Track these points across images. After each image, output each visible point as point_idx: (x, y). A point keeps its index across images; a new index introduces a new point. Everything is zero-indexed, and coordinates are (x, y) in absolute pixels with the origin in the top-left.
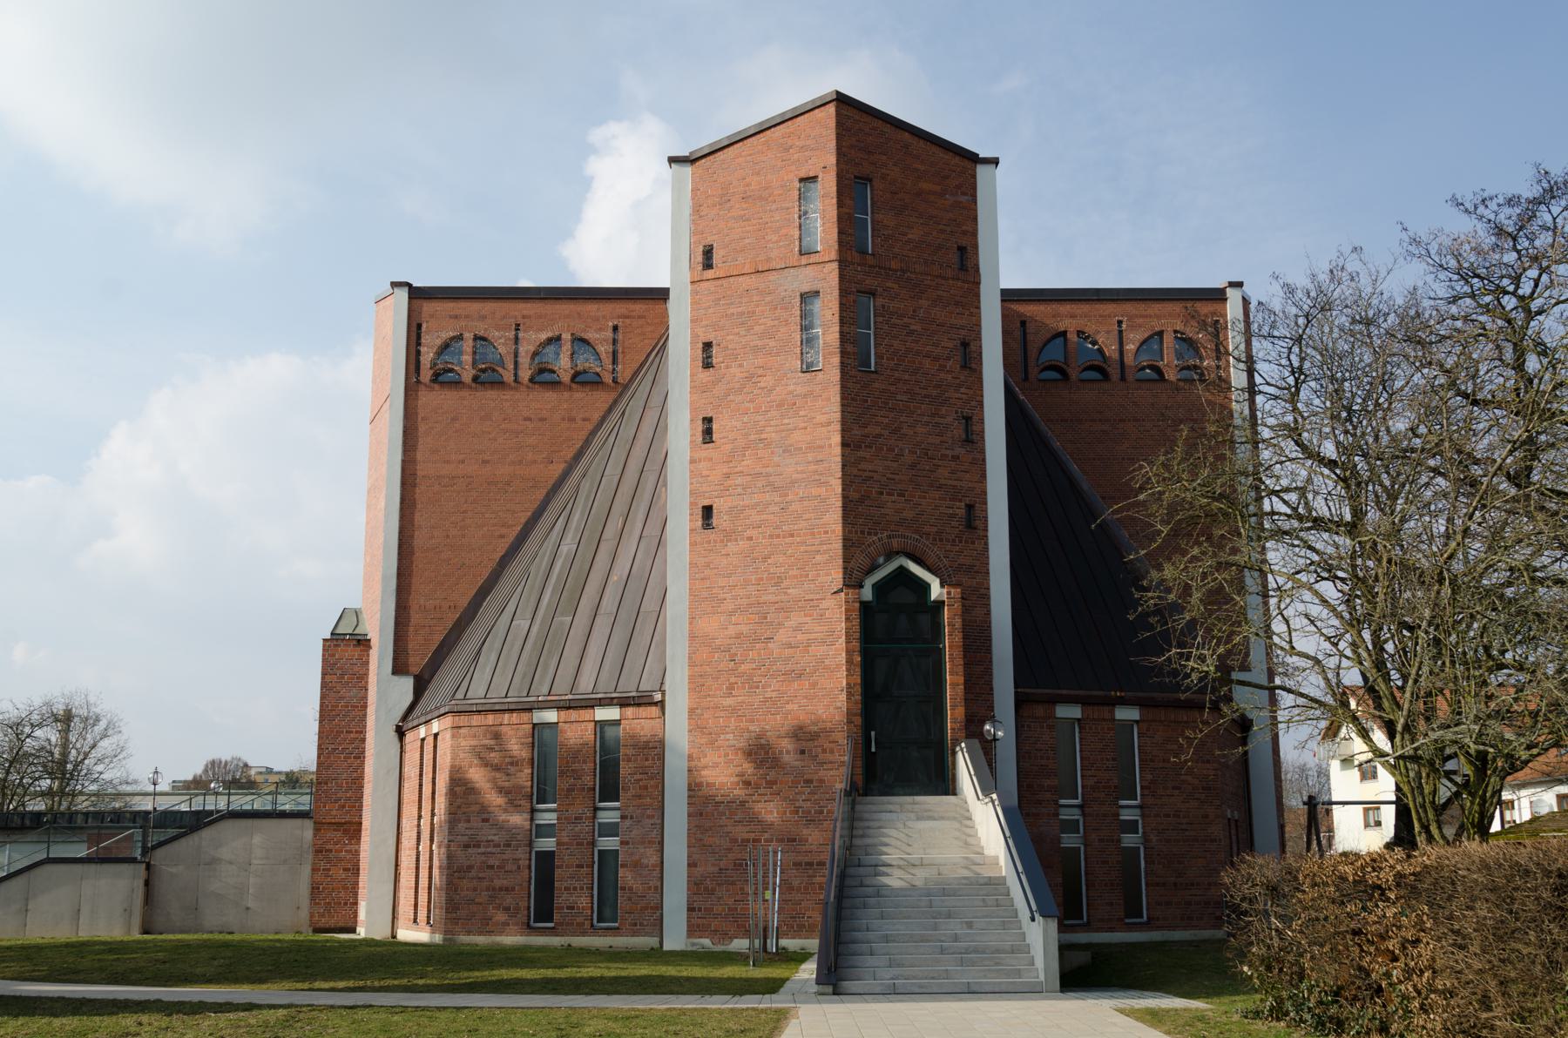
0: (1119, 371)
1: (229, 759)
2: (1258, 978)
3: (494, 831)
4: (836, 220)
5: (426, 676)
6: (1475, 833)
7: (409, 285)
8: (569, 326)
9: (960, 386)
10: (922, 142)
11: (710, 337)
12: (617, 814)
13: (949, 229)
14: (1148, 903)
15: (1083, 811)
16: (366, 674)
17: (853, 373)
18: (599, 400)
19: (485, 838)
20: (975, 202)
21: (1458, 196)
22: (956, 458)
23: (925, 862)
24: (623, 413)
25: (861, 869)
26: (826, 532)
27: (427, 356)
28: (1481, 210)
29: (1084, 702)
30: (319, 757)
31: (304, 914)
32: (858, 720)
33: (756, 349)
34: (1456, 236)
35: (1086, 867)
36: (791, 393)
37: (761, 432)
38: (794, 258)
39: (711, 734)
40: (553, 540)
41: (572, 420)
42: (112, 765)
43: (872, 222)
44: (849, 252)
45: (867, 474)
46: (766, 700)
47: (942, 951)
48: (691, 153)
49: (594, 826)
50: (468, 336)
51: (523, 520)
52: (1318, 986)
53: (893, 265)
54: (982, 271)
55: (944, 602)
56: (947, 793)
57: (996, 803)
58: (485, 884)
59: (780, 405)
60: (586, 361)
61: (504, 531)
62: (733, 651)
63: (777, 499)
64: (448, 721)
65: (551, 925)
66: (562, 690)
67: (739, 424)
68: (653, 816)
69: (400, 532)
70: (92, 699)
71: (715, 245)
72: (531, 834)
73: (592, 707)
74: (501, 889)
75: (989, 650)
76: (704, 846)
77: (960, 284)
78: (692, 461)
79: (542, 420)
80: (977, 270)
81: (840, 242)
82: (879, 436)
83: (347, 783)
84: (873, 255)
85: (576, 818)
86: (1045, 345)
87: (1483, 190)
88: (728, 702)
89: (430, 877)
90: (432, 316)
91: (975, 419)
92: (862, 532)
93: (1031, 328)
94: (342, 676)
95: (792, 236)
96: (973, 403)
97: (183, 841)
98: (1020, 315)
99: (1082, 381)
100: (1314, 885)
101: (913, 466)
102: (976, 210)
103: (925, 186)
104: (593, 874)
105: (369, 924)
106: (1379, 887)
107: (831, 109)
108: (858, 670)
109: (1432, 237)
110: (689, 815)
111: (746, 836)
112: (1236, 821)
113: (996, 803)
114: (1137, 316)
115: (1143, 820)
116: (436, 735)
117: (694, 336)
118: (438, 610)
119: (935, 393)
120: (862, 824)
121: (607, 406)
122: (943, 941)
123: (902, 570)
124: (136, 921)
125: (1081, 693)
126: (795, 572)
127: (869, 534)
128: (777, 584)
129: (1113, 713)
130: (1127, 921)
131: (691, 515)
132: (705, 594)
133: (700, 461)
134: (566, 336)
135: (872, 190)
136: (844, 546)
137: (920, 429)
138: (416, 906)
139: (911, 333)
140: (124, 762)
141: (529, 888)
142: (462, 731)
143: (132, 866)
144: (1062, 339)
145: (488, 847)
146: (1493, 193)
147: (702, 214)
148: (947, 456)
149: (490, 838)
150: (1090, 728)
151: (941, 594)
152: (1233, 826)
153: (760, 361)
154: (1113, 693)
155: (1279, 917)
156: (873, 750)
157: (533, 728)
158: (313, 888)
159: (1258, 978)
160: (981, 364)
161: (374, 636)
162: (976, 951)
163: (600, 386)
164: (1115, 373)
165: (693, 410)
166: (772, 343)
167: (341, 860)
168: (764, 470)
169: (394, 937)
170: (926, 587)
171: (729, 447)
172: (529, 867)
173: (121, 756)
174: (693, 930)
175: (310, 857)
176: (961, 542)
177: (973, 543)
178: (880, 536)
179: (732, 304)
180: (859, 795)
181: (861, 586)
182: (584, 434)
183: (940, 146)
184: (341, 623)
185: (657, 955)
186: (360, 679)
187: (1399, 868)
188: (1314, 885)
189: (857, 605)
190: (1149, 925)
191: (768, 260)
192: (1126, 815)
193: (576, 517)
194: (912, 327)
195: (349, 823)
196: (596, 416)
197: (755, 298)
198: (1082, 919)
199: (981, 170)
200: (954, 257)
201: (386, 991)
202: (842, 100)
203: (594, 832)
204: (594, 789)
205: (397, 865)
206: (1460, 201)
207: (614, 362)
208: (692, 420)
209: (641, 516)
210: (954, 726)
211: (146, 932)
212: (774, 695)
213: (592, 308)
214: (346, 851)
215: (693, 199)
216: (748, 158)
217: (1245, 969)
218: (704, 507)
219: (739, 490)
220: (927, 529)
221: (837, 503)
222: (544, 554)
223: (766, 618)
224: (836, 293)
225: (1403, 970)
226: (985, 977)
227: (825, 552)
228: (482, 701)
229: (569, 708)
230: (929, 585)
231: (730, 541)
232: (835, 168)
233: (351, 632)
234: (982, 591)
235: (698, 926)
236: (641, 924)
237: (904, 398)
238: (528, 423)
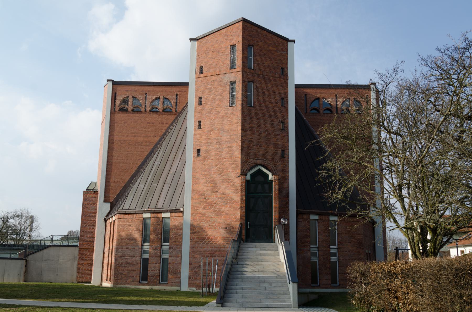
0: (336, 111)
1: (75, 231)
2: (357, 305)
3: (130, 252)
4: (241, 58)
5: (114, 203)
6: (432, 256)
7: (113, 81)
8: (162, 94)
9: (281, 112)
10: (270, 34)
11: (201, 95)
12: (168, 247)
14: (339, 280)
15: (318, 249)
16: (97, 202)
17: (246, 107)
18: (171, 117)
19: (127, 254)
20: (287, 54)
21: (439, 47)
22: (279, 135)
23: (259, 264)
24: (178, 121)
25: (238, 265)
26: (236, 158)
27: (118, 103)
28: (446, 52)
29: (319, 214)
30: (81, 228)
31: (75, 277)
32: (244, 218)
33: (215, 99)
34: (436, 57)
35: (319, 267)
36: (226, 113)
37: (216, 125)
38: (228, 70)
39: (198, 222)
40: (153, 160)
41: (162, 123)
42: (35, 231)
43: (253, 59)
44: (245, 68)
45: (249, 139)
46: (215, 211)
47: (260, 293)
48: (197, 37)
49: (161, 251)
50: (131, 97)
51: (146, 155)
52: (376, 308)
53: (260, 73)
55: (273, 180)
56: (272, 242)
57: (283, 245)
58: (127, 268)
59: (222, 117)
60: (167, 104)
61: (140, 158)
62: (205, 195)
63: (221, 147)
64: (117, 216)
65: (147, 282)
66: (152, 208)
67: (209, 123)
68: (179, 248)
69: (108, 158)
70: (29, 211)
71: (203, 66)
72: (141, 253)
73: (161, 213)
74: (131, 270)
75: (288, 197)
76: (195, 258)
77: (281, 79)
78: (195, 135)
79: (153, 123)
80: (287, 75)
81: (243, 65)
82: (254, 127)
83: (90, 236)
84: (253, 69)
85: (155, 248)
86: (312, 102)
87: (447, 45)
88: (203, 212)
89: (111, 266)
90: (119, 90)
91: (286, 123)
92: (247, 158)
93: (308, 96)
94: (89, 202)
95: (227, 63)
96: (285, 118)
97: (38, 254)
99: (324, 113)
100: (375, 273)
101: (265, 137)
103: (270, 48)
104: (160, 266)
105: (95, 281)
106: (395, 274)
107: (241, 23)
108: (244, 202)
109: (428, 58)
110: (190, 248)
111: (208, 255)
112: (370, 254)
113: (283, 245)
114: (342, 93)
115: (338, 253)
116: (114, 221)
117: (196, 95)
118: (118, 182)
119: (272, 114)
120: (242, 251)
121: (173, 119)
122: (261, 290)
123: (260, 170)
124: (22, 278)
125: (319, 211)
126: (226, 170)
127: (250, 158)
128: (220, 174)
129: (329, 218)
130: (332, 285)
131: (194, 152)
132: (197, 177)
133: (197, 135)
134: (161, 97)
135: (253, 49)
136: (241, 162)
138: (107, 275)
139: (265, 95)
140: (39, 230)
141: (140, 270)
142: (121, 220)
143: (21, 261)
144: (318, 100)
145: (128, 256)
146: (450, 46)
147: (200, 56)
148: (276, 134)
149: (128, 254)
150: (321, 223)
151: (272, 178)
152: (368, 255)
153: (216, 103)
154: (329, 212)
155: (365, 284)
156: (249, 228)
157: (143, 219)
158: (78, 269)
159: (357, 305)
160: (288, 105)
161: (99, 190)
162: (272, 293)
163: (171, 113)
164: (334, 110)
165: (195, 118)
166: (220, 97)
167: (87, 260)
168: (217, 138)
169: (101, 285)
170: (267, 176)
171: (206, 130)
172: (140, 263)
173: (38, 229)
174: (190, 285)
175: (77, 259)
176: (280, 162)
179: (208, 85)
180: (244, 242)
181: (246, 175)
182: (166, 128)
183: (276, 36)
184: (90, 186)
185: (178, 293)
186: (95, 204)
187: (402, 267)
188: (375, 273)
189: (245, 181)
190: (339, 286)
191: (220, 71)
192: (333, 251)
193: (161, 153)
194: (266, 93)
195: (90, 249)
196: (170, 122)
197: (216, 83)
198: (317, 284)
200: (280, 71)
201: (84, 303)
202: (244, 20)
203: (161, 253)
204: (161, 239)
205: (103, 262)
206: (440, 49)
207: (176, 106)
208: (195, 122)
209: (181, 153)
211: (25, 282)
212: (218, 209)
213: (170, 89)
214: (88, 258)
215: (197, 52)
216: (215, 39)
217: (353, 301)
218: (198, 149)
219: (209, 144)
220: (269, 157)
221: (239, 148)
222: (150, 164)
223: (216, 185)
224: (241, 81)
225: (402, 304)
226: (273, 302)
227: (235, 164)
228: (128, 210)
229: (154, 213)
230: (268, 175)
231: (205, 160)
232: (242, 42)
233: (92, 189)
234: (286, 178)
235: (192, 283)
236: (175, 283)
237: (263, 115)
238: (148, 124)
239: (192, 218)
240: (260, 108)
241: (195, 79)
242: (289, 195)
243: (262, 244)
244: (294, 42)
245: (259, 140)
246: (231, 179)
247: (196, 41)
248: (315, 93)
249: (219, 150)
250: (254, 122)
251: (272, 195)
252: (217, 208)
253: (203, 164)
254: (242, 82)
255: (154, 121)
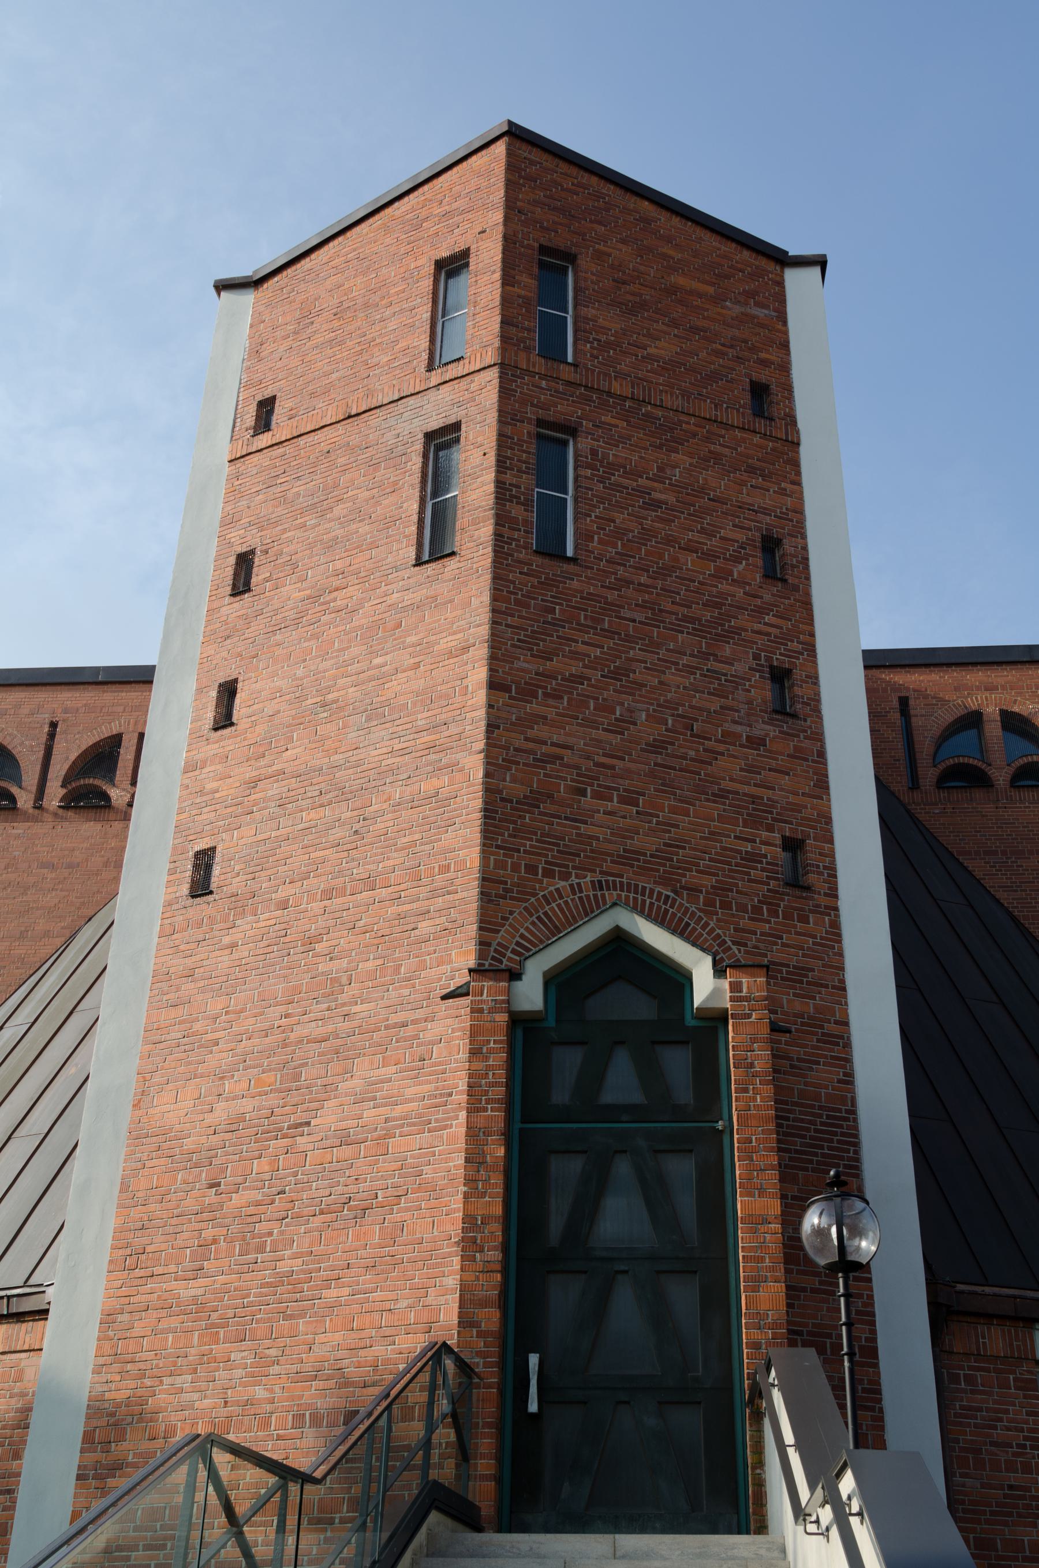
9: (760, 612)
13: (731, 352)
20: (782, 317)
22: (756, 742)
33: (331, 545)
37: (329, 690)
38: (417, 378)
43: (575, 323)
48: (255, 272)
53: (616, 387)
54: (801, 425)
56: (741, 1528)
77: (756, 439)
79: (70, 866)
80: (792, 421)
82: (580, 679)
84: (575, 365)
91: (798, 674)
92: (531, 869)
93: (916, 707)
96: (794, 645)
98: (896, 688)
101: (657, 747)
102: (786, 333)
107: (500, 149)
108: (497, 1180)
127: (548, 873)
131: (172, 872)
137: (671, 676)
139: (656, 504)
151: (716, 992)
156: (533, 1407)
170: (682, 980)
176: (774, 913)
177: (804, 919)
178: (574, 880)
181: (515, 976)
189: (502, 1018)
197: (342, 461)
199: (796, 281)
200: (762, 692)
210: (757, 1335)
220: (691, 878)
223: (297, 1077)
230: (691, 974)
232: (501, 228)
234: (830, 1027)
237: (639, 616)
239: (107, 1346)
240: (620, 571)
241: (226, 468)
242: (858, 1160)
243: (629, 1541)
244: (817, 270)
245: (614, 761)
246: (404, 1025)
247: (252, 290)
248: (956, 689)
249: (337, 834)
250: (582, 648)
251: (720, 1125)
252: (295, 1257)
253: (226, 940)
254: (500, 421)
255: (77, 853)
